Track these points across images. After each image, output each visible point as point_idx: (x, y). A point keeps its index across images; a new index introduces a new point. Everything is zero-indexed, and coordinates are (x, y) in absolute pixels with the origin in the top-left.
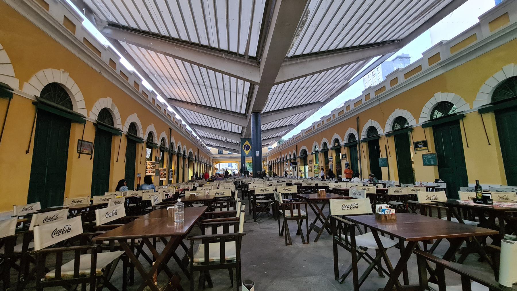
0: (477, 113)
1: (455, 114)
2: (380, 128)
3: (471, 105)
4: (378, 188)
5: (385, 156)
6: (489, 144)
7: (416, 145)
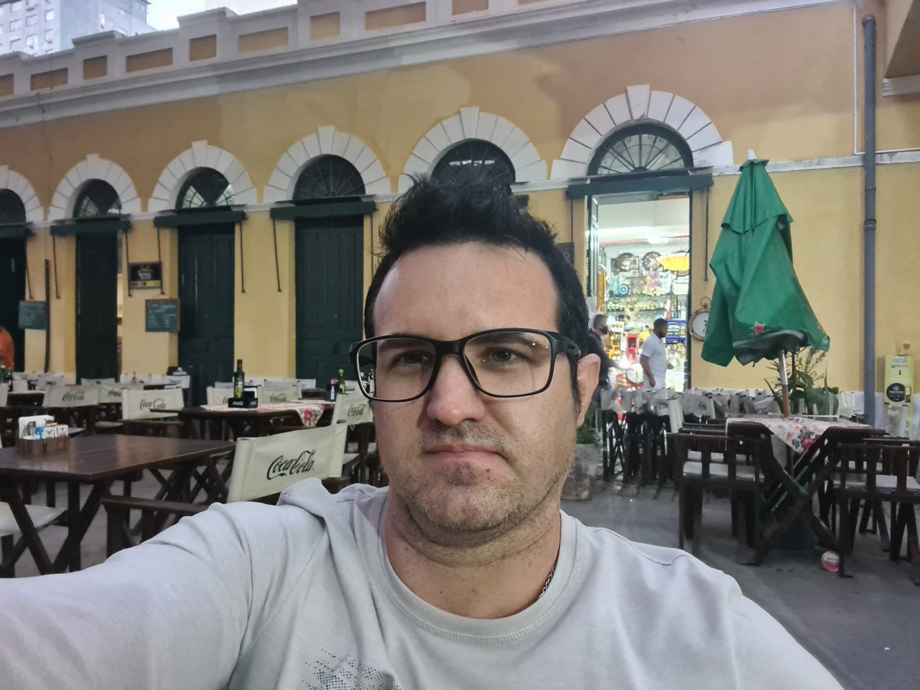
0: (267, 216)
1: (227, 208)
2: (36, 201)
3: (260, 192)
4: (15, 392)
5: (40, 296)
6: (279, 290)
7: (134, 272)
